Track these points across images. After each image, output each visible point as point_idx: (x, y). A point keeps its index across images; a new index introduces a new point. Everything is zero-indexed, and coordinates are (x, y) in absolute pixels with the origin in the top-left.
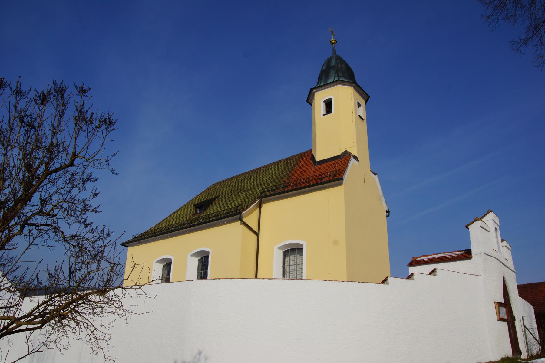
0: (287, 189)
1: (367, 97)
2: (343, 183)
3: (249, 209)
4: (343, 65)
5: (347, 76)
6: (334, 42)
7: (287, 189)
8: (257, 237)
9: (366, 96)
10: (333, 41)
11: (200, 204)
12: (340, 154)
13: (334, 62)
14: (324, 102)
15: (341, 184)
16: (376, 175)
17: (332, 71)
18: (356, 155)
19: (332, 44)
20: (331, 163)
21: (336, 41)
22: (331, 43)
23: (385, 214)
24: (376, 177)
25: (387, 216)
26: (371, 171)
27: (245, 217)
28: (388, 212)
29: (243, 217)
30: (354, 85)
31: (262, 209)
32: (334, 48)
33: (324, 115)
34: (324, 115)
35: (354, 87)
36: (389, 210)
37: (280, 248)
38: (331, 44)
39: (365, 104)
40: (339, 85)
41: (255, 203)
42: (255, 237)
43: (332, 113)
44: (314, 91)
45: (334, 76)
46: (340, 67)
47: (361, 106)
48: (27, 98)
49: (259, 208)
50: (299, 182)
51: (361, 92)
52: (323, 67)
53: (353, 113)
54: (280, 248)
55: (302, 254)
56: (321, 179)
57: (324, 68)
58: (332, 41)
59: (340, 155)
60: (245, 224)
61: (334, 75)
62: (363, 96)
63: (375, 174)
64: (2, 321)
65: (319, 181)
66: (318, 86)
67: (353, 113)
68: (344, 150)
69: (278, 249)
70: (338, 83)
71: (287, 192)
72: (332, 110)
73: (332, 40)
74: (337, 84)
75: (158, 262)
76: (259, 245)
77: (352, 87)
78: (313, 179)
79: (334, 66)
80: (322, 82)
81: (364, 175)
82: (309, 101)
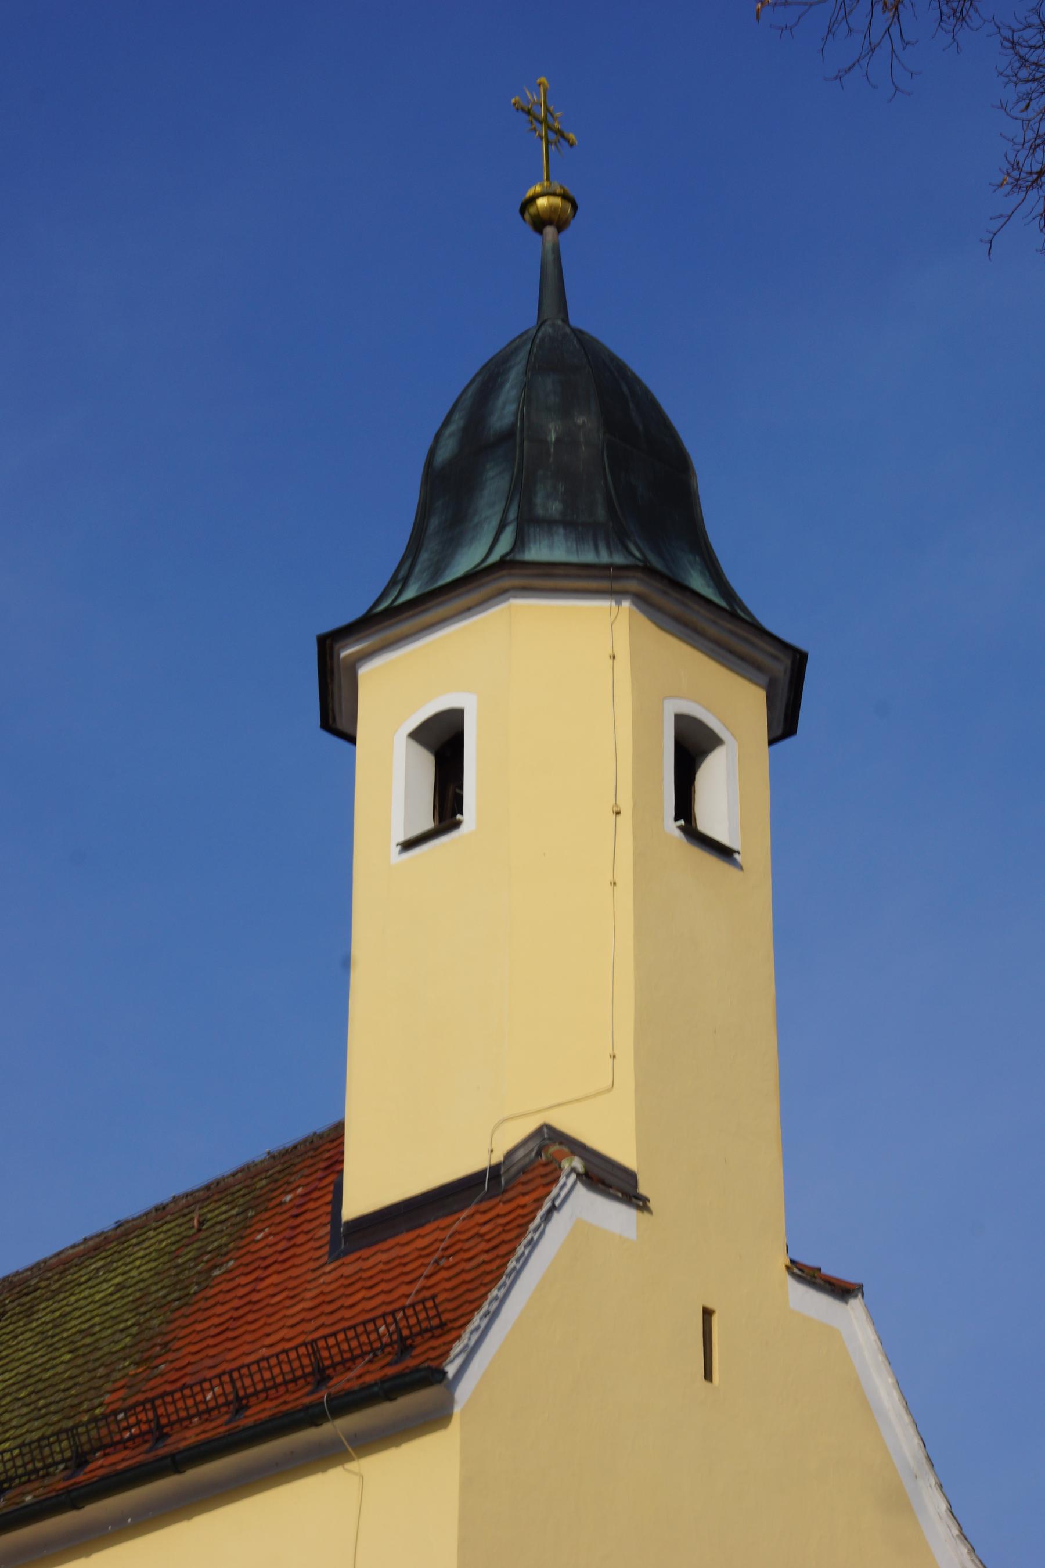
0: (100, 1465)
1: (788, 662)
2: (457, 1410)
4: (580, 421)
5: (601, 513)
6: (552, 209)
7: (100, 1465)
9: (772, 650)
10: (542, 202)
11: (92, 1484)
13: (513, 393)
14: (419, 735)
16: (856, 1304)
17: (491, 474)
18: (624, 1152)
19: (539, 224)
20: (460, 1220)
21: (565, 197)
22: (527, 216)
30: (633, 585)
32: (550, 257)
33: (408, 845)
34: (408, 845)
35: (641, 601)
38: (528, 229)
43: (464, 829)
44: (345, 653)
45: (495, 522)
46: (553, 437)
47: (713, 741)
50: (187, 1409)
51: (712, 630)
52: (438, 436)
56: (321, 1376)
57: (444, 453)
58: (533, 199)
59: (495, 1171)
61: (499, 508)
62: (743, 658)
65: (301, 1397)
66: (386, 610)
67: (618, 813)
68: (527, 1127)
70: (506, 583)
71: (177, 1463)
73: (530, 193)
74: (502, 594)
77: (626, 604)
78: (273, 1378)
79: (508, 435)
80: (417, 569)
82: (342, 725)
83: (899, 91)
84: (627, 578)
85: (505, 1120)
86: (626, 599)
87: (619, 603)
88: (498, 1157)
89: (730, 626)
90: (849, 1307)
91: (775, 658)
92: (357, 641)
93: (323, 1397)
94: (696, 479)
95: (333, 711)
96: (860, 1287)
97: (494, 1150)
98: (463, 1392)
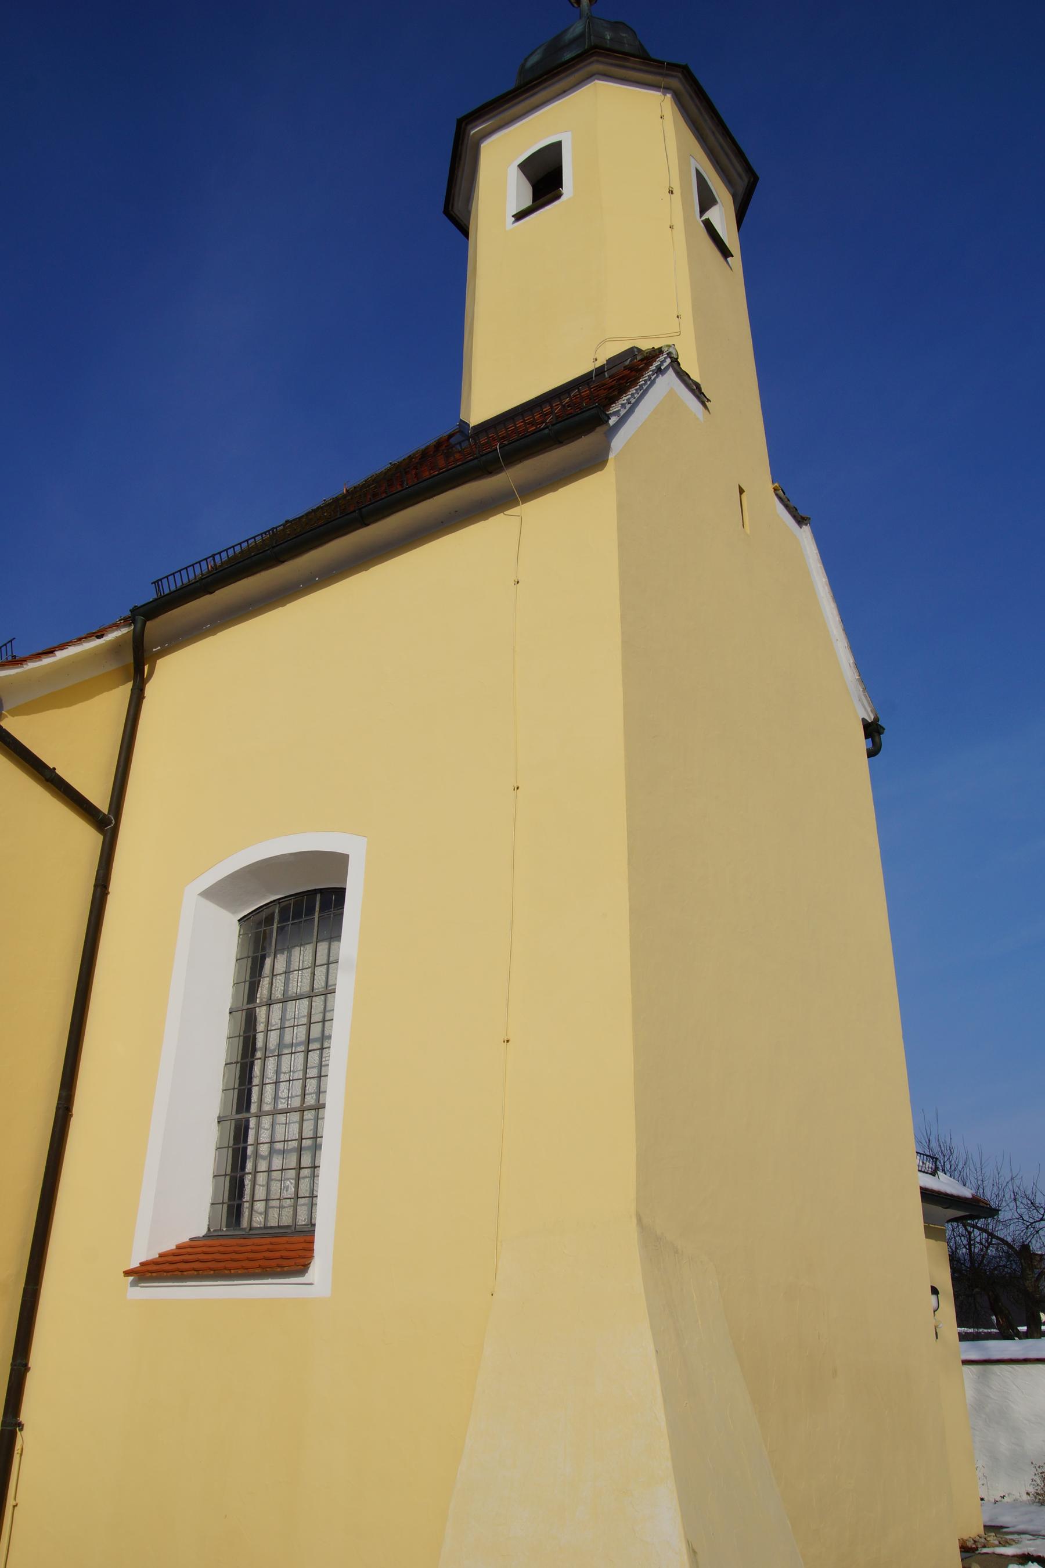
3: (46, 661)
8: (100, 838)
9: (740, 170)
12: (598, 364)
15: (595, 462)
23: (861, 744)
24: (806, 530)
25: (871, 754)
26: (775, 490)
27: (16, 712)
28: (872, 730)
29: (7, 706)
31: (150, 689)
33: (520, 216)
34: (520, 216)
36: (876, 719)
37: (218, 894)
39: (738, 232)
40: (597, 82)
41: (100, 637)
42: (90, 839)
43: (563, 198)
44: (472, 133)
46: (609, 38)
48: (504, 1042)
49: (130, 684)
51: (711, 138)
53: (671, 192)
54: (218, 894)
55: (332, 929)
60: (1031, 1361)
63: (801, 521)
64: (282, 1173)
69: (199, 897)
72: (560, 184)
75: (213, 894)
76: (112, 888)
77: (669, 96)
81: (741, 491)
83: (290, 967)
84: (672, 76)
85: (605, 341)
86: (669, 93)
87: (665, 94)
88: (601, 361)
89: (721, 139)
90: (802, 530)
91: (741, 178)
92: (483, 122)
93: (291, 904)
94: (223, 1081)
95: (453, 199)
96: (810, 519)
97: (598, 358)
98: (618, 442)
